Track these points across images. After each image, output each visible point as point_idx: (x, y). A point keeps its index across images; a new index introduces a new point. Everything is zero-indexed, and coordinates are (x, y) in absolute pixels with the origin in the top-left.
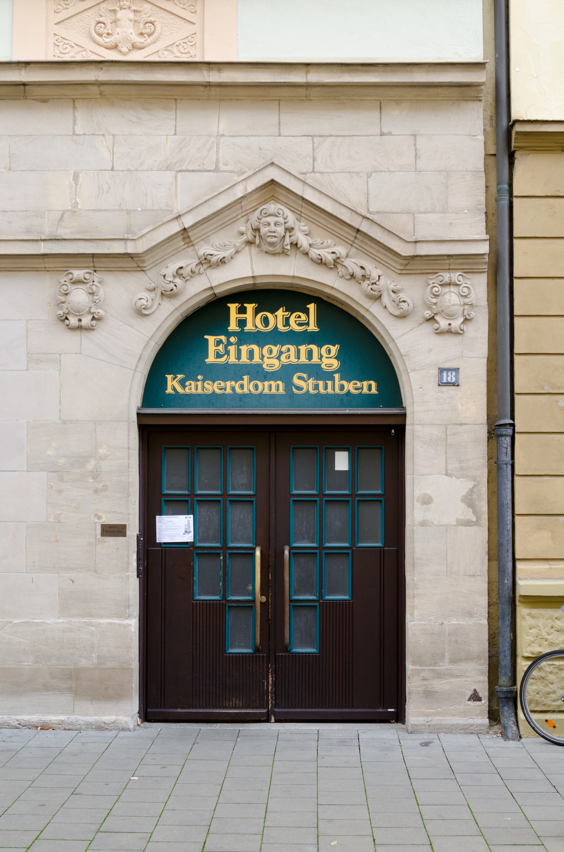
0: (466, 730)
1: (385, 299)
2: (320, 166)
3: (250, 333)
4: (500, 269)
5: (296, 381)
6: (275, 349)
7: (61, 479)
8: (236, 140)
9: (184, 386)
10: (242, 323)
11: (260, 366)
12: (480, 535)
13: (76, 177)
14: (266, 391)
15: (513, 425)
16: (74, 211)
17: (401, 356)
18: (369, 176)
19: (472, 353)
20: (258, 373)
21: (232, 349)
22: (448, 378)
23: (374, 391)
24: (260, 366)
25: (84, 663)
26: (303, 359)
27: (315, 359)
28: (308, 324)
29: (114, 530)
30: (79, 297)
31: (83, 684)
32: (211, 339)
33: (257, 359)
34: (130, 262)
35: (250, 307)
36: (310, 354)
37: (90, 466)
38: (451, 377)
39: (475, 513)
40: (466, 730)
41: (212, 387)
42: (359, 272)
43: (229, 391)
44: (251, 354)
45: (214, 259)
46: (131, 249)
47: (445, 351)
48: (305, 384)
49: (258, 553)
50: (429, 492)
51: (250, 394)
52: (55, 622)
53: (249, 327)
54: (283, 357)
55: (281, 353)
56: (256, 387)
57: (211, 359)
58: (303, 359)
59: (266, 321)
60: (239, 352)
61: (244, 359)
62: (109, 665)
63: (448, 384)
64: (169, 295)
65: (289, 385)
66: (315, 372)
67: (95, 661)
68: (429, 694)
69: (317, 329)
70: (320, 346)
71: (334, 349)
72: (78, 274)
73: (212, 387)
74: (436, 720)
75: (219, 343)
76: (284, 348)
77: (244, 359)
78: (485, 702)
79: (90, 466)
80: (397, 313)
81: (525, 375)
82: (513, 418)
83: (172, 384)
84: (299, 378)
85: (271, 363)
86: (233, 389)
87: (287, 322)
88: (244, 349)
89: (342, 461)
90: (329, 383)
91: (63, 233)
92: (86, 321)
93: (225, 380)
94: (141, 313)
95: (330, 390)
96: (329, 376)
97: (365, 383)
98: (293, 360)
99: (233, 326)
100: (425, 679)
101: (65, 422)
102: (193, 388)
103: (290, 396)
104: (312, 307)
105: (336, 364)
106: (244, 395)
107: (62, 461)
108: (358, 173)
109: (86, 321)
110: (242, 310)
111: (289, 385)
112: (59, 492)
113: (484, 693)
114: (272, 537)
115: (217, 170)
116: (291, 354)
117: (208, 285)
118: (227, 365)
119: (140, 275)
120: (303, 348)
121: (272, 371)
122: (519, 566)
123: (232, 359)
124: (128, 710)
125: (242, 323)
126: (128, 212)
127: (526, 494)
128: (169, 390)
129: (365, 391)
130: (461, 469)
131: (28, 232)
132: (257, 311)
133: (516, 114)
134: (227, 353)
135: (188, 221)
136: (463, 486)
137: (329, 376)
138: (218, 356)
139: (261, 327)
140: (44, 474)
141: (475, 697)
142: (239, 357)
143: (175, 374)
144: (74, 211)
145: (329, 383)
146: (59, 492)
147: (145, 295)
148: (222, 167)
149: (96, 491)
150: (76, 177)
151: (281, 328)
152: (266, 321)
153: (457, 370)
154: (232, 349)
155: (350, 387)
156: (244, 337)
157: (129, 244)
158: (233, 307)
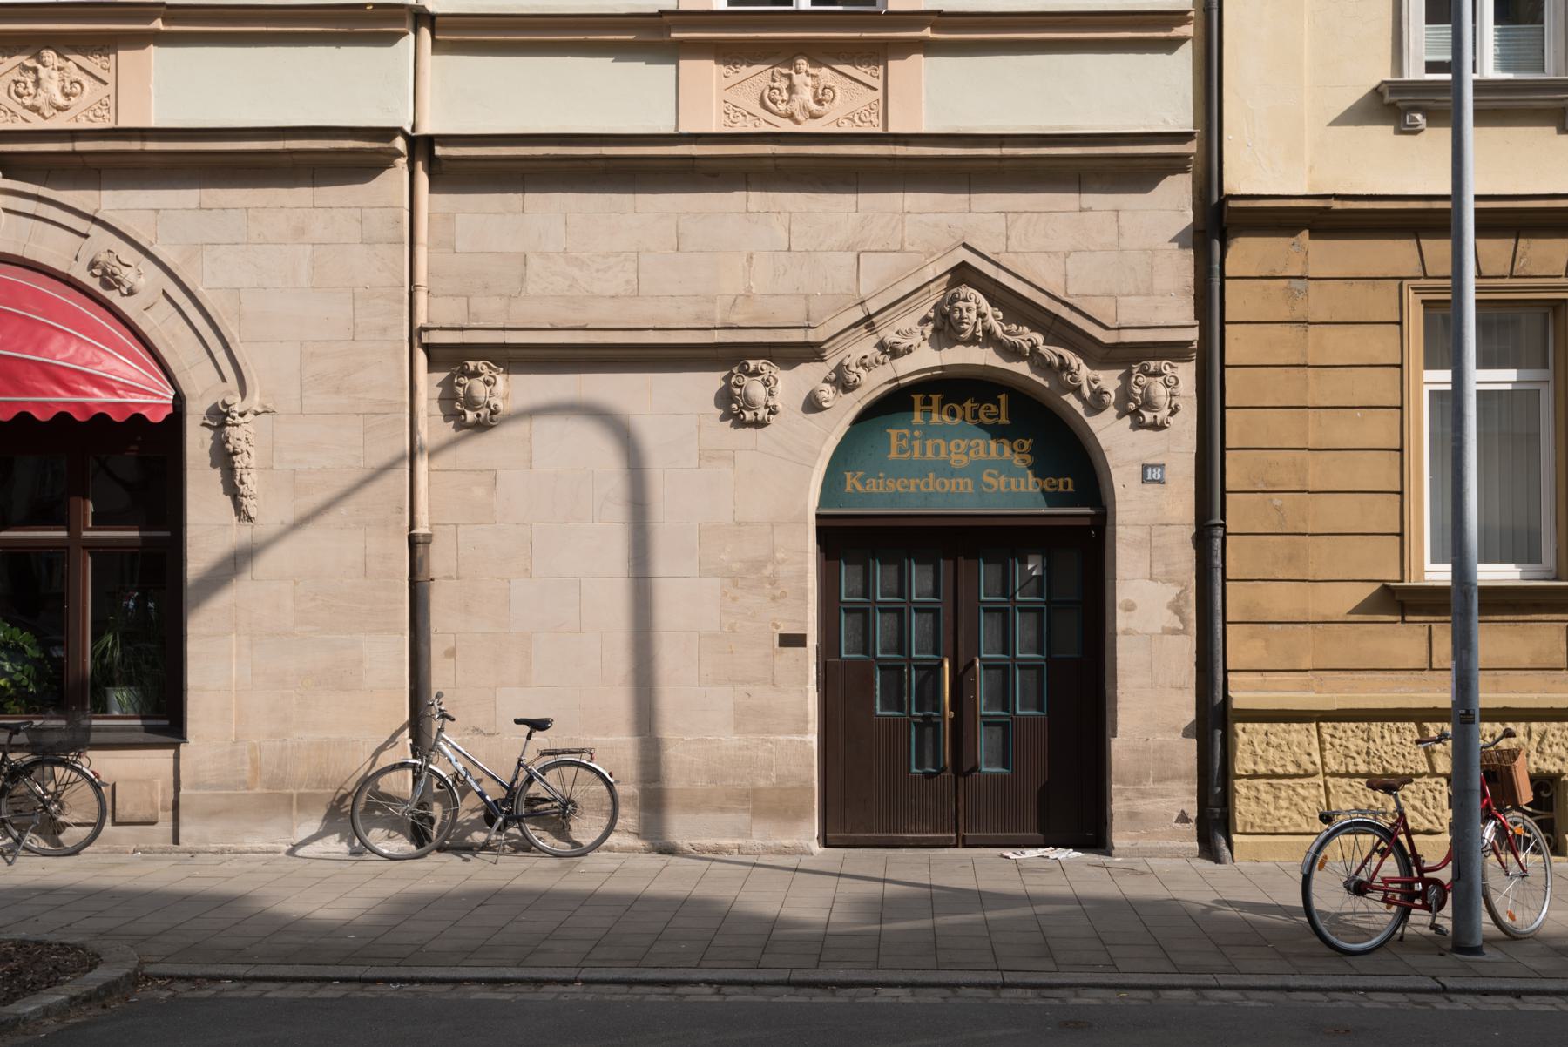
0: (1175, 854)
2: (1014, 244)
4: (1208, 359)
5: (985, 478)
6: (963, 444)
7: (735, 585)
8: (923, 217)
9: (864, 485)
11: (946, 462)
12: (1189, 644)
14: (954, 488)
15: (1224, 526)
18: (1067, 255)
19: (1177, 445)
21: (916, 444)
22: (1150, 474)
23: (1070, 488)
24: (946, 462)
25: (762, 783)
28: (999, 416)
29: (793, 640)
31: (769, 805)
35: (936, 398)
37: (767, 572)
38: (1156, 474)
39: (1182, 620)
40: (1175, 854)
41: (896, 486)
43: (913, 489)
44: (937, 449)
45: (901, 347)
46: (812, 337)
47: (1146, 445)
49: (947, 665)
50: (1132, 598)
52: (730, 740)
54: (972, 453)
55: (970, 448)
56: (943, 484)
57: (893, 455)
60: (924, 447)
62: (789, 785)
63: (1153, 481)
65: (978, 482)
67: (774, 780)
68: (1132, 815)
69: (1008, 422)
71: (1027, 444)
73: (896, 486)
74: (1142, 843)
75: (901, 437)
76: (973, 443)
79: (767, 572)
81: (1237, 471)
83: (852, 482)
84: (990, 475)
86: (917, 486)
88: (929, 443)
90: (1022, 481)
91: (736, 319)
92: (762, 413)
93: (909, 478)
95: (1022, 488)
97: (1061, 481)
98: (983, 455)
100: (1128, 799)
101: (739, 524)
102: (874, 486)
104: (1003, 398)
107: (736, 567)
108: (1055, 253)
111: (978, 482)
112: (734, 599)
115: (902, 250)
117: (893, 376)
121: (978, 474)
122: (1231, 677)
123: (917, 454)
124: (807, 835)
126: (807, 297)
127: (1237, 599)
128: (849, 489)
129: (1061, 488)
130: (1167, 573)
131: (698, 318)
132: (943, 403)
133: (1227, 190)
134: (911, 448)
135: (873, 307)
136: (1172, 591)
138: (901, 451)
140: (718, 580)
141: (1183, 818)
143: (855, 472)
145: (1022, 481)
146: (734, 599)
148: (907, 247)
149: (774, 598)
150: (750, 257)
153: (1162, 466)
154: (916, 444)
157: (810, 332)
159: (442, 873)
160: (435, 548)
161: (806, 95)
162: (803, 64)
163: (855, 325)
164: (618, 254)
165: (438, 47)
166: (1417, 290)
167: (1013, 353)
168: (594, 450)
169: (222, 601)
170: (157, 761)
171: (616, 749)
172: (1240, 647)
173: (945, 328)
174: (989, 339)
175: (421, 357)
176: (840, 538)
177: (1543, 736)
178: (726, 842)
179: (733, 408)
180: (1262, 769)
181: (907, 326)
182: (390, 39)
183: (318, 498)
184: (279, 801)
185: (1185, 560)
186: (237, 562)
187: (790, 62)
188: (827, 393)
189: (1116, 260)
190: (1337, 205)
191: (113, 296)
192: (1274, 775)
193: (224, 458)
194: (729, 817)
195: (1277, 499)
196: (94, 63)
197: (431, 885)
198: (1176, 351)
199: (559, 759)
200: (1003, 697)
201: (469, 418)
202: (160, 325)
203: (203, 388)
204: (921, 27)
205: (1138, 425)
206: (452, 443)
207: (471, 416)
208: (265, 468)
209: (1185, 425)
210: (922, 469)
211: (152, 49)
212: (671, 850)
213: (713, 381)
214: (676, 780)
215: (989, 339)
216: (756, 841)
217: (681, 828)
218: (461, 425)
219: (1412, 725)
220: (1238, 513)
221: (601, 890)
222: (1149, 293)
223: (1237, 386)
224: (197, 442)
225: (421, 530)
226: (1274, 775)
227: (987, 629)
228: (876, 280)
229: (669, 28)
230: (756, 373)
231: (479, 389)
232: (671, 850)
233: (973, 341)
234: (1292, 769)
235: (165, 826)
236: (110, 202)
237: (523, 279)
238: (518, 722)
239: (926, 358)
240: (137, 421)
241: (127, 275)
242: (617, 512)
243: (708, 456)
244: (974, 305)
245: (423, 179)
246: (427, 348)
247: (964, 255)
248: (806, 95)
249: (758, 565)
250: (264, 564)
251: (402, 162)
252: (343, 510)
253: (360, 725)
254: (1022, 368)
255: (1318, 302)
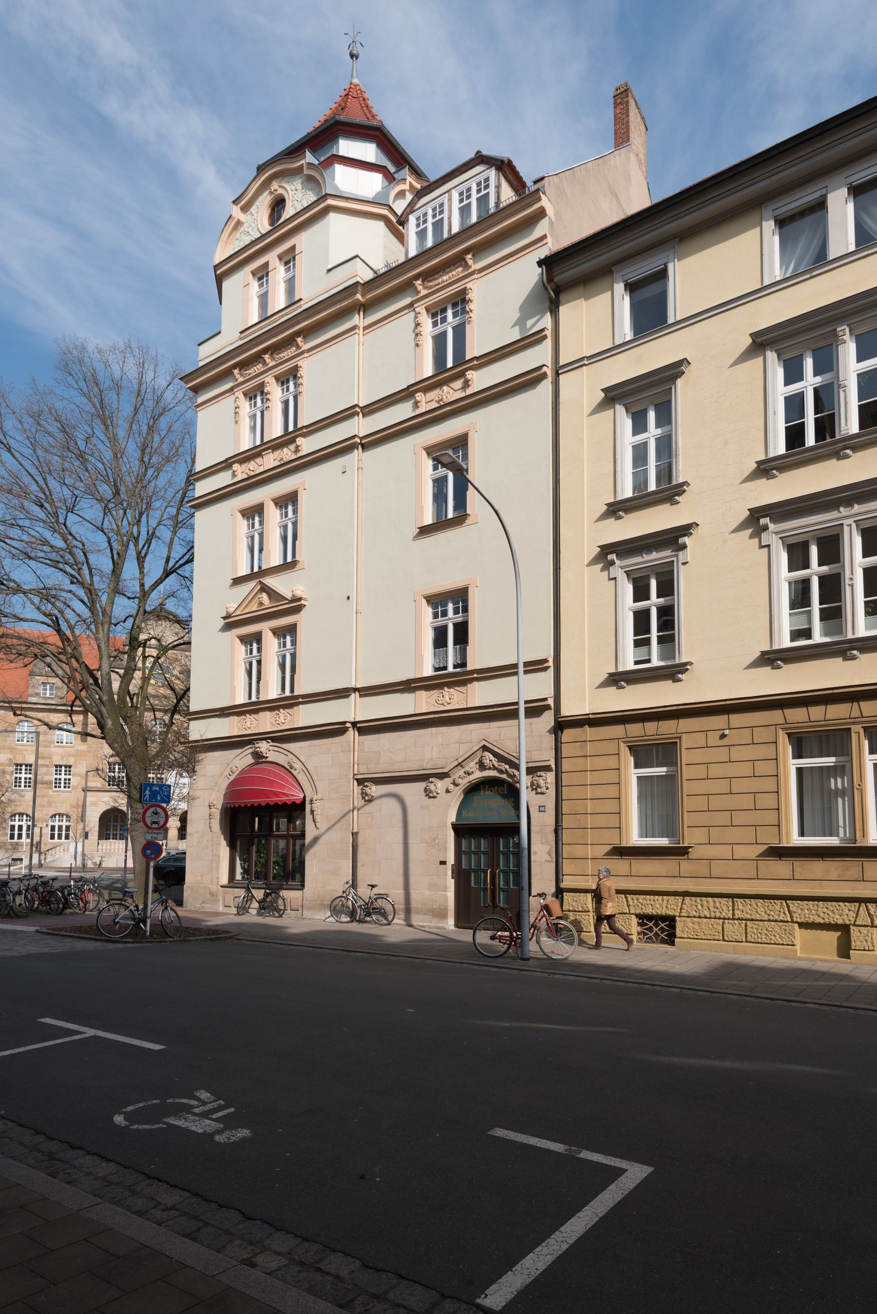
38: (542, 809)
46: (445, 771)
52: (427, 893)
92: (435, 794)
121: (492, 809)
127: (566, 851)
135: (460, 760)
136: (547, 848)
159: (355, 927)
160: (359, 835)
161: (447, 698)
162: (446, 689)
163: (457, 766)
165: (361, 696)
166: (783, 729)
167: (501, 771)
168: (393, 806)
169: (312, 851)
170: (298, 894)
171: (397, 895)
172: (567, 867)
173: (482, 766)
174: (494, 768)
175: (355, 782)
176: (459, 830)
177: (668, 901)
178: (425, 924)
179: (428, 793)
180: (571, 909)
181: (472, 766)
182: (348, 696)
183: (333, 822)
184: (322, 907)
185: (552, 837)
186: (315, 840)
187: (443, 689)
188: (451, 787)
189: (528, 740)
190: (591, 716)
191: (292, 771)
192: (575, 911)
193: (312, 812)
194: (426, 917)
195: (578, 817)
196: (290, 711)
197: (258, 921)
198: (547, 768)
199: (381, 896)
200: (507, 882)
201: (368, 800)
202: (301, 777)
203: (309, 795)
204: (473, 674)
205: (537, 793)
206: (364, 806)
207: (367, 798)
208: (322, 815)
209: (552, 793)
211: (301, 706)
212: (410, 926)
213: (422, 785)
214: (414, 905)
215: (494, 768)
216: (433, 924)
217: (416, 920)
218: (366, 801)
219: (623, 896)
220: (566, 822)
221: (571, 958)
222: (540, 750)
223: (566, 779)
224: (308, 807)
226: (575, 911)
228: (463, 751)
229: (410, 684)
230: (540, 776)
231: (368, 790)
232: (410, 926)
233: (490, 769)
234: (581, 909)
235: (300, 911)
236: (292, 746)
239: (478, 775)
240: (294, 803)
241: (294, 765)
242: (400, 824)
244: (488, 757)
245: (356, 733)
246: (357, 780)
247: (484, 743)
248: (447, 698)
250: (321, 841)
251: (351, 729)
252: (337, 825)
253: (337, 885)
254: (504, 776)
255: (589, 749)
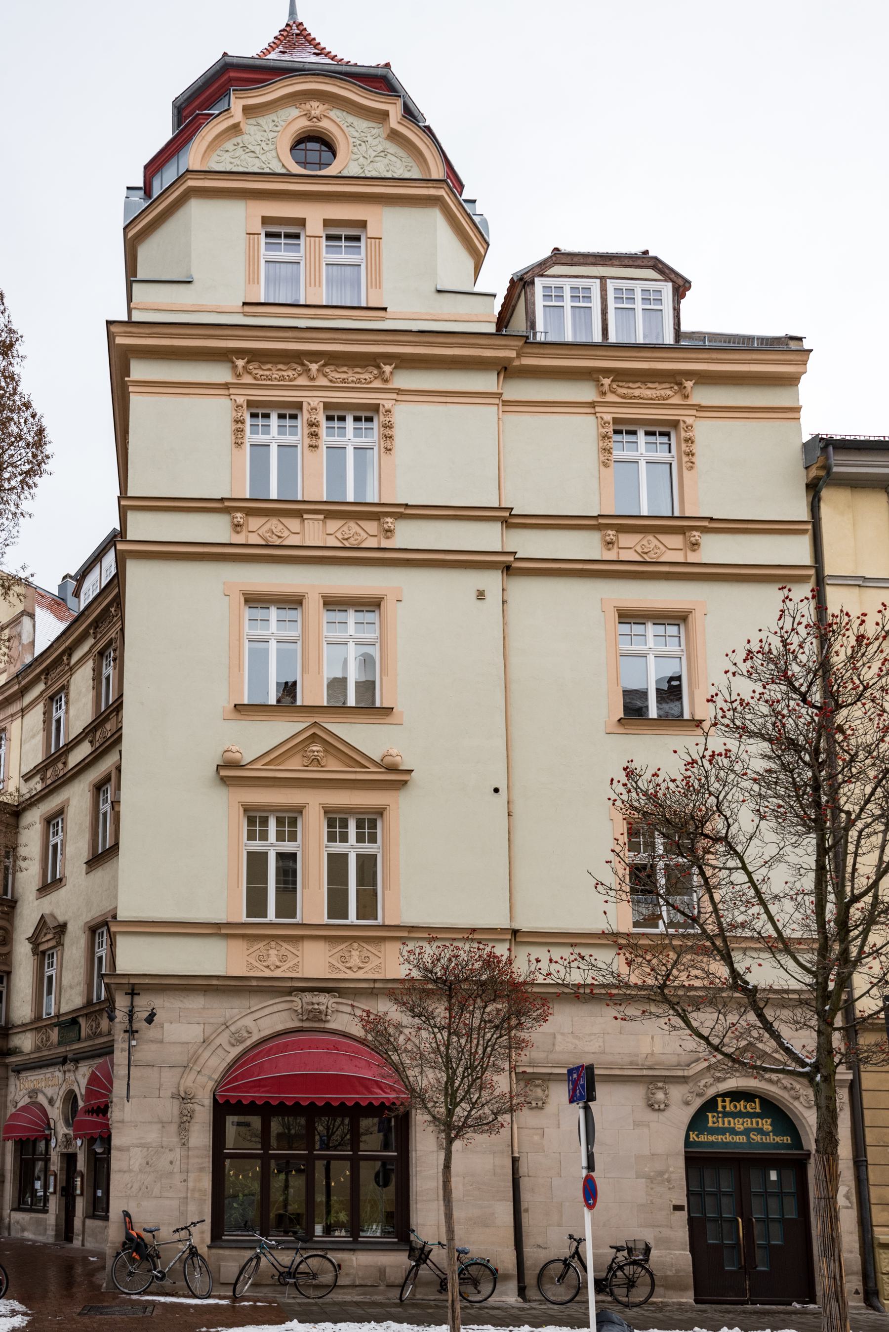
1: (801, 1099)
3: (728, 1112)
6: (741, 1120)
10: (724, 1107)
11: (734, 1128)
13: (652, 1038)
16: (652, 1054)
17: (810, 1126)
20: (733, 1132)
23: (789, 1141)
24: (734, 1128)
25: (669, 1273)
26: (755, 1125)
27: (760, 1126)
29: (677, 1208)
30: (660, 1096)
32: (710, 1115)
33: (732, 1125)
34: (684, 1080)
35: (728, 1100)
36: (757, 1123)
37: (666, 1176)
39: (850, 1202)
41: (712, 1138)
42: (789, 1086)
44: (729, 1122)
48: (756, 1138)
51: (730, 1142)
53: (728, 1109)
57: (710, 1124)
58: (755, 1125)
59: (735, 1107)
61: (726, 1125)
62: (681, 1274)
64: (699, 1095)
65: (748, 1137)
66: (761, 1131)
70: (762, 1119)
71: (769, 1121)
72: (660, 1084)
73: (712, 1138)
75: (714, 1117)
77: (726, 1125)
78: (862, 1295)
79: (666, 1176)
80: (807, 1105)
82: (866, 1157)
85: (739, 1127)
87: (746, 1108)
88: (726, 1120)
89: (773, 1176)
92: (662, 1106)
94: (687, 1103)
96: (766, 1134)
98: (750, 1125)
99: (720, 1109)
102: (703, 1138)
103: (750, 1143)
104: (757, 1100)
105: (770, 1128)
106: (727, 1143)
107: (652, 1174)
109: (662, 1106)
110: (724, 1101)
111: (748, 1137)
113: (861, 1290)
114: (743, 1210)
116: (749, 1123)
118: (718, 1128)
119: (686, 1085)
120: (754, 1120)
121: (744, 1132)
123: (721, 1125)
124: (688, 1298)
125: (724, 1107)
127: (874, 1194)
128: (691, 1139)
132: (731, 1102)
134: (718, 1121)
137: (766, 1134)
138: (714, 1123)
139: (733, 1109)
141: (857, 1292)
142: (724, 1124)
144: (652, 1054)
146: (652, 1189)
147: (689, 1095)
149: (669, 1189)
150: (652, 1038)
151: (743, 1110)
152: (735, 1107)
154: (720, 1120)
155: (778, 1139)
156: (726, 1114)
158: (719, 1099)
164: (595, 1034)
176: (697, 1161)
210: (722, 1131)
223: (867, 1099)
225: (516, 1155)
227: (756, 1203)
237: (554, 1045)
238: (612, 1247)
243: (637, 1124)
249: (661, 1173)
